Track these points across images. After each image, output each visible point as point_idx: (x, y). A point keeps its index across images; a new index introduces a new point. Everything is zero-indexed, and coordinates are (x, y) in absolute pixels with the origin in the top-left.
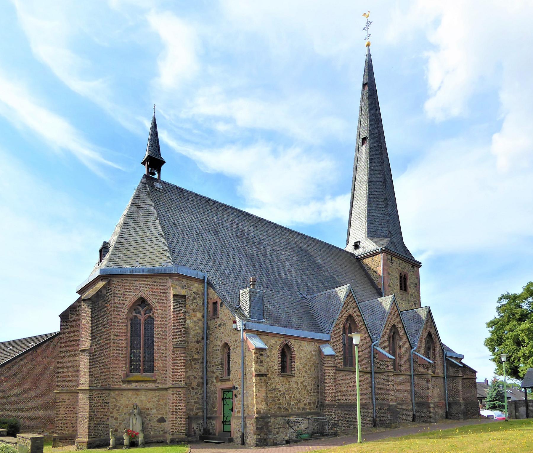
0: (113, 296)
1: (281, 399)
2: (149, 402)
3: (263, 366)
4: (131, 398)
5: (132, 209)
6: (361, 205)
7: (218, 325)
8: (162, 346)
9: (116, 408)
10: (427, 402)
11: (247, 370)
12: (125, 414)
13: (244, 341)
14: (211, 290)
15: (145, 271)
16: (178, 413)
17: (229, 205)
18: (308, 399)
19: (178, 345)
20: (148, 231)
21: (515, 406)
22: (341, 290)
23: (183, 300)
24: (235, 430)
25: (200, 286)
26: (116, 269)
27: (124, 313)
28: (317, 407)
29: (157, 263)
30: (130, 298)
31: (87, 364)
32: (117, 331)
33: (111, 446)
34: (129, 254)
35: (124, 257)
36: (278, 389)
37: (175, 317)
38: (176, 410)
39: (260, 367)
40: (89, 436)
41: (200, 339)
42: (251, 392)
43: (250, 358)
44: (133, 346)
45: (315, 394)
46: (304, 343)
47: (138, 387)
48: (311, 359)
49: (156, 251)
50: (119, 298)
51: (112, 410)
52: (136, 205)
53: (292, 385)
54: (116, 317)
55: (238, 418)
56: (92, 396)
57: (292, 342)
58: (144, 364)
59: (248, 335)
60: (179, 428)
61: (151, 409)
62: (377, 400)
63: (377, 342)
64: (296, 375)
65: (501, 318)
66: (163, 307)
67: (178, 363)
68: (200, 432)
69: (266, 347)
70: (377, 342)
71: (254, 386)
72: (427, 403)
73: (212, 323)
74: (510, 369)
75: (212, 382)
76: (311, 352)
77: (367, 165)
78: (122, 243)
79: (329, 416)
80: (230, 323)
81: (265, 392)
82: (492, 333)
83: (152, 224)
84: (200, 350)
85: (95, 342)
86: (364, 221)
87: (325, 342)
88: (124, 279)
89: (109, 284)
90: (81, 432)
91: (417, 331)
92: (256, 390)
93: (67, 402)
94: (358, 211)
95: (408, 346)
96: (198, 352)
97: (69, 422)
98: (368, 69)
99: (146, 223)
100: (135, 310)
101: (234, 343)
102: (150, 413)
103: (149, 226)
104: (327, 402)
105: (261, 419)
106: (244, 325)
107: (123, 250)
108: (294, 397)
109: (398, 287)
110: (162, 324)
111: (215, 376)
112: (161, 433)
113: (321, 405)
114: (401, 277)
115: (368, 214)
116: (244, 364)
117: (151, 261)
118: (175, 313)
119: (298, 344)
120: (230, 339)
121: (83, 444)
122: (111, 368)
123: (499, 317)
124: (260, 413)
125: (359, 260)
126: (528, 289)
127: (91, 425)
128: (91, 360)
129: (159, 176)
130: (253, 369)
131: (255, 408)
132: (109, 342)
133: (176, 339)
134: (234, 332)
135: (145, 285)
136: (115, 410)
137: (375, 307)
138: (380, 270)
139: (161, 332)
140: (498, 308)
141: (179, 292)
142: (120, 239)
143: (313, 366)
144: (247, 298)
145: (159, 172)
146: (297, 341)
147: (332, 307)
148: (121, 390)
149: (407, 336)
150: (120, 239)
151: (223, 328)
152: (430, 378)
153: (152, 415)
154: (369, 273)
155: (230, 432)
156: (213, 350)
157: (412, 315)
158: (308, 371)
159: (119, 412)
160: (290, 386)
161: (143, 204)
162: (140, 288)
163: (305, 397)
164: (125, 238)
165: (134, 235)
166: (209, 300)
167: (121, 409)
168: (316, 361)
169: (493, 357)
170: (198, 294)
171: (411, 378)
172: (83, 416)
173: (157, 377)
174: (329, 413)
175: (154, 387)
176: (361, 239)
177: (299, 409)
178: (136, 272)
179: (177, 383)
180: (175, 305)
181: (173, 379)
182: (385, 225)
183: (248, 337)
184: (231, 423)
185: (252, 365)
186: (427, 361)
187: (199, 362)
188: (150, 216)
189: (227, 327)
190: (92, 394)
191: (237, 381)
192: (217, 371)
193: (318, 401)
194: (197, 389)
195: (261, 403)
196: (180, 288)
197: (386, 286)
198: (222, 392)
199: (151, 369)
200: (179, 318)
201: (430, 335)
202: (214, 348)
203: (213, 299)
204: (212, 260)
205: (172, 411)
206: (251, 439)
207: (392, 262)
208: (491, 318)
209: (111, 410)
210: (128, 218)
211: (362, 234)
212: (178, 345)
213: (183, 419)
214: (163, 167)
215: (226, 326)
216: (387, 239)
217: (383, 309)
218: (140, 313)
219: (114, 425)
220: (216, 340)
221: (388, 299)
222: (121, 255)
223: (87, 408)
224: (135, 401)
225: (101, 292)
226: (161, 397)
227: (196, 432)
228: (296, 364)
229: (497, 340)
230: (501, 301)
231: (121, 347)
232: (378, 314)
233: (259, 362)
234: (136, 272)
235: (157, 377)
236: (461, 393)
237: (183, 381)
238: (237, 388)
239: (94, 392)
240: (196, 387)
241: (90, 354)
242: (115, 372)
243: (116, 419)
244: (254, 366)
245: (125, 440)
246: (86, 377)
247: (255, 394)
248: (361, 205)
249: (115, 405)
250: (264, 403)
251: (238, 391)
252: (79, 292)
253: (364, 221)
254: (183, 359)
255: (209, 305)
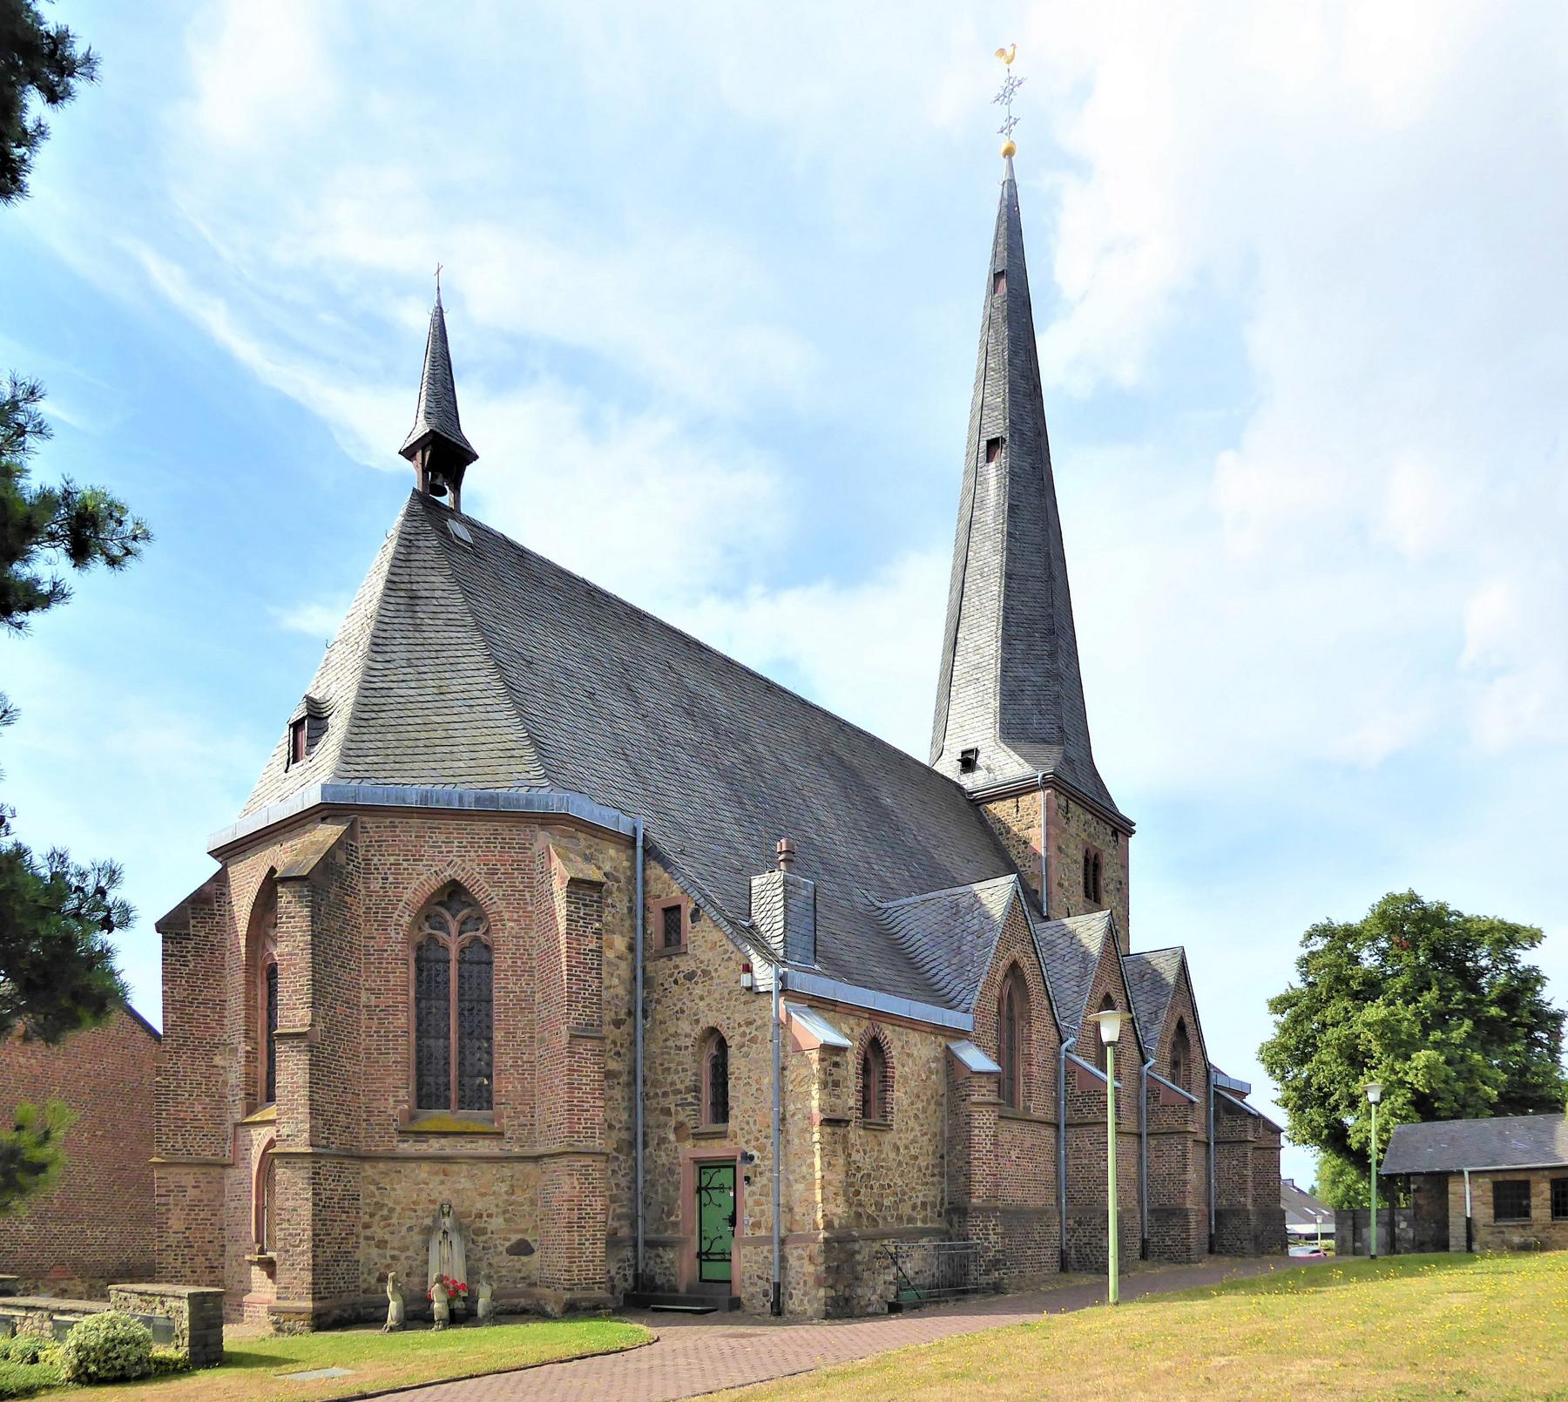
0: (362, 871)
1: (863, 1191)
2: (483, 1195)
3: (838, 1097)
4: (427, 1184)
5: (392, 600)
6: (981, 642)
7: (682, 975)
8: (519, 1032)
9: (380, 1213)
10: (1182, 1206)
11: (791, 1107)
12: (410, 1229)
13: (783, 1026)
14: (656, 870)
15: (466, 799)
16: (584, 1227)
17: (650, 613)
18: (920, 1191)
19: (583, 1031)
20: (454, 675)
21: (1354, 1225)
22: (991, 891)
23: (596, 895)
24: (747, 1275)
25: (623, 856)
26: (368, 791)
27: (402, 926)
28: (940, 1215)
29: (497, 778)
30: (418, 882)
31: (302, 1078)
32: (379, 979)
33: (393, 1323)
34: (406, 743)
35: (389, 752)
36: (855, 1162)
37: (574, 945)
38: (579, 1218)
39: (833, 1099)
40: (314, 1294)
41: (622, 1016)
42: (804, 1168)
43: (804, 1072)
44: (426, 1026)
45: (935, 1179)
46: (914, 1037)
47: (448, 1152)
48: (929, 1082)
49: (489, 739)
50: (383, 879)
51: (367, 1217)
52: (403, 586)
53: (885, 1151)
54: (375, 938)
55: (758, 1242)
56: (319, 1174)
57: (887, 1032)
58: (460, 1082)
59: (791, 1007)
60: (589, 1270)
61: (490, 1216)
62: (1070, 1199)
63: (1072, 1040)
64: (895, 1127)
65: (1306, 990)
66: (521, 913)
67: (584, 1082)
68: (625, 1285)
69: (847, 1043)
70: (1072, 1040)
71: (818, 1153)
72: (1179, 1209)
73: (662, 969)
74: (1326, 1127)
75: (663, 1140)
76: (928, 1062)
77: (1003, 524)
78: (376, 708)
79: (980, 1239)
80: (725, 972)
81: (844, 1169)
82: (1284, 1030)
83: (465, 653)
84: (622, 1045)
85: (321, 1012)
86: (990, 690)
87: (960, 1035)
88: (397, 821)
89: (350, 833)
90: (287, 1281)
91: (1153, 1016)
92: (822, 1163)
93: (191, 1192)
94: (974, 659)
95: (1136, 1054)
96: (618, 1054)
97: (200, 1254)
98: (1008, 229)
99: (444, 648)
100: (428, 918)
101: (742, 1029)
102: (485, 1228)
103: (456, 660)
104: (974, 1200)
105: (836, 1245)
106: (781, 979)
107: (383, 729)
108: (889, 1186)
109: (1081, 890)
110: (519, 964)
111: (673, 1123)
112: (519, 1286)
113: (956, 1211)
114: (1086, 860)
115: (1002, 671)
116: (781, 1091)
117: (479, 770)
118: (574, 933)
119: (899, 1040)
120: (728, 1018)
121: (297, 1317)
122: (361, 1093)
123: (1302, 985)
124: (833, 1227)
125: (975, 804)
126: (1385, 912)
127: (319, 1260)
128: (314, 1065)
129: (457, 501)
130: (815, 1104)
131: (820, 1214)
132: (355, 1012)
133: (577, 1013)
134: (743, 999)
135: (464, 844)
136: (377, 1217)
137: (1058, 941)
138: (1038, 839)
139: (517, 990)
140: (1304, 963)
141: (581, 871)
142: (367, 693)
143: (933, 1102)
144: (775, 899)
145: (456, 488)
146: (897, 1028)
147: (969, 938)
148: (393, 1158)
149: (1135, 1027)
150: (367, 693)
151: (700, 985)
152: (1190, 1144)
153: (492, 1233)
154: (1004, 843)
155: (730, 1282)
156: (667, 1047)
157: (1136, 970)
158: (921, 1116)
159: (389, 1225)
160: (882, 1157)
161: (427, 586)
162: (448, 852)
163: (913, 1188)
164: (384, 692)
165: (413, 684)
166: (650, 901)
167: (395, 1215)
168: (940, 1088)
169: (1279, 1095)
170: (618, 881)
171: (1140, 1143)
172: (290, 1235)
173: (505, 1121)
174: (981, 1230)
175: (497, 1150)
176: (981, 742)
177: (900, 1218)
178: (437, 801)
179: (581, 1141)
180: (572, 909)
181: (569, 1127)
182: (1049, 707)
183: (792, 1014)
184: (735, 1257)
185: (808, 1093)
186: (1187, 1098)
187: (621, 1081)
188: (453, 629)
189: (716, 981)
190: (320, 1168)
191: (751, 1137)
192: (679, 1108)
193: (942, 1199)
194: (617, 1159)
195: (835, 1200)
196: (579, 859)
197: (1054, 887)
198: (697, 1170)
199: (480, 1098)
200: (585, 950)
201: (1181, 1027)
202: (671, 1043)
203: (664, 896)
204: (642, 780)
205: (569, 1223)
206: (806, 1294)
207: (1069, 815)
208: (1279, 990)
209: (366, 1218)
210: (385, 627)
211: (984, 727)
212: (583, 1031)
213: (598, 1245)
214: (471, 471)
215: (712, 978)
216: (1056, 749)
217: (1083, 949)
218: (443, 927)
219: (376, 1264)
220: (677, 1019)
221: (1094, 923)
222: (380, 744)
223: (306, 1212)
224: (440, 1193)
225: (334, 858)
226: (520, 1183)
227: (616, 1282)
228: (896, 1094)
229: (1297, 1049)
230: (1311, 942)
231: (392, 1029)
232: (1067, 964)
233: (830, 1085)
234: (437, 801)
235: (505, 1121)
236: (1250, 1185)
237: (597, 1135)
238: (751, 1158)
239: (323, 1162)
240: (615, 1154)
241: (311, 1048)
242: (375, 1104)
243: (382, 1244)
244: (817, 1096)
245: (436, 1305)
246: (300, 1117)
247: (818, 1175)
248: (981, 642)
249: (376, 1203)
250: (841, 1200)
251: (756, 1166)
252: (215, 853)
253: (990, 690)
254: (596, 1069)
255: (650, 915)
